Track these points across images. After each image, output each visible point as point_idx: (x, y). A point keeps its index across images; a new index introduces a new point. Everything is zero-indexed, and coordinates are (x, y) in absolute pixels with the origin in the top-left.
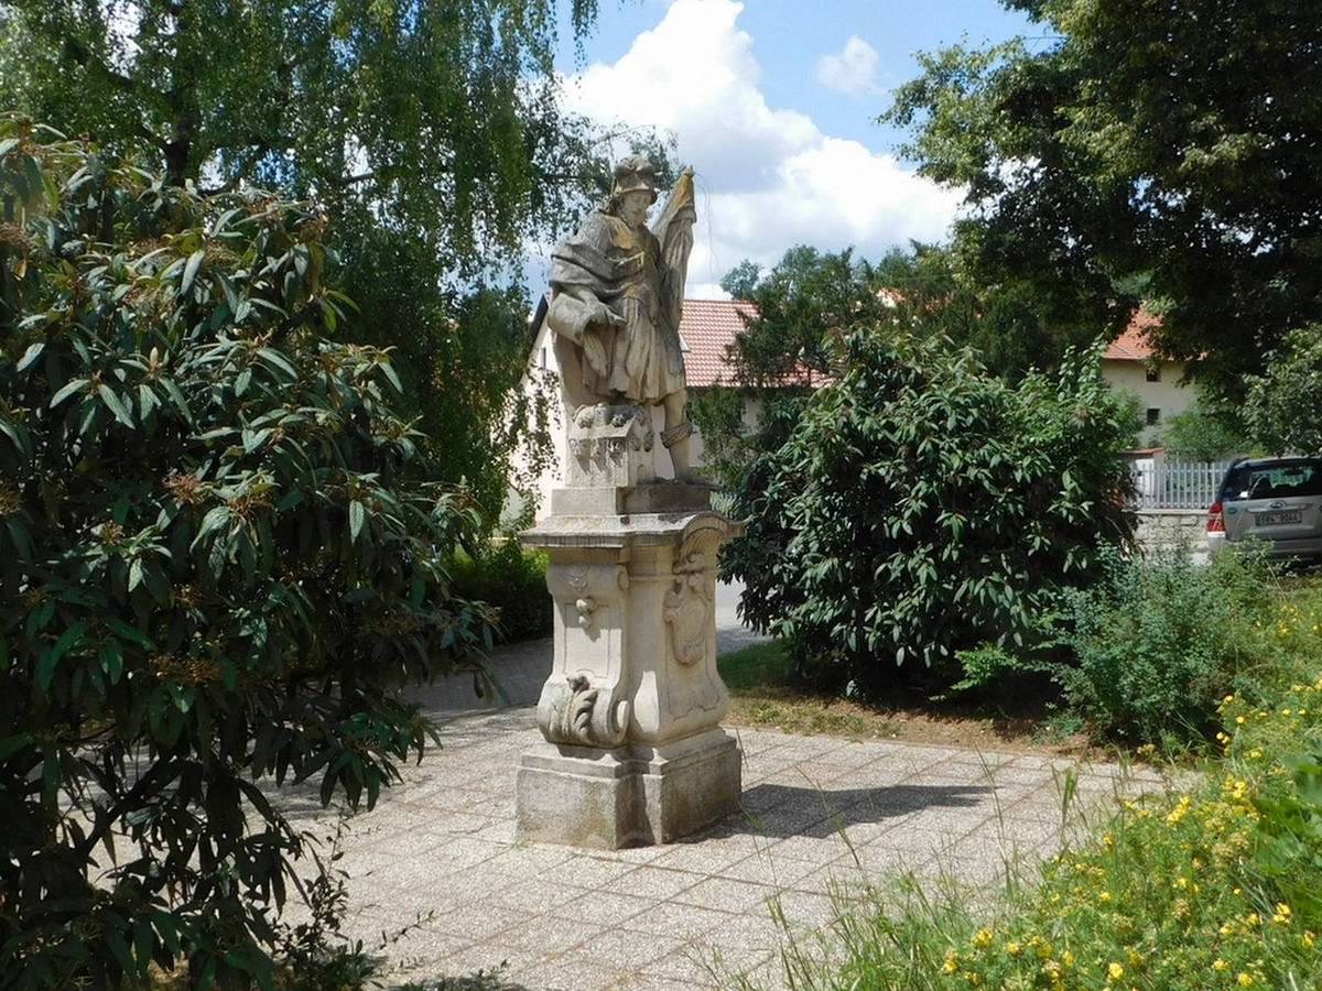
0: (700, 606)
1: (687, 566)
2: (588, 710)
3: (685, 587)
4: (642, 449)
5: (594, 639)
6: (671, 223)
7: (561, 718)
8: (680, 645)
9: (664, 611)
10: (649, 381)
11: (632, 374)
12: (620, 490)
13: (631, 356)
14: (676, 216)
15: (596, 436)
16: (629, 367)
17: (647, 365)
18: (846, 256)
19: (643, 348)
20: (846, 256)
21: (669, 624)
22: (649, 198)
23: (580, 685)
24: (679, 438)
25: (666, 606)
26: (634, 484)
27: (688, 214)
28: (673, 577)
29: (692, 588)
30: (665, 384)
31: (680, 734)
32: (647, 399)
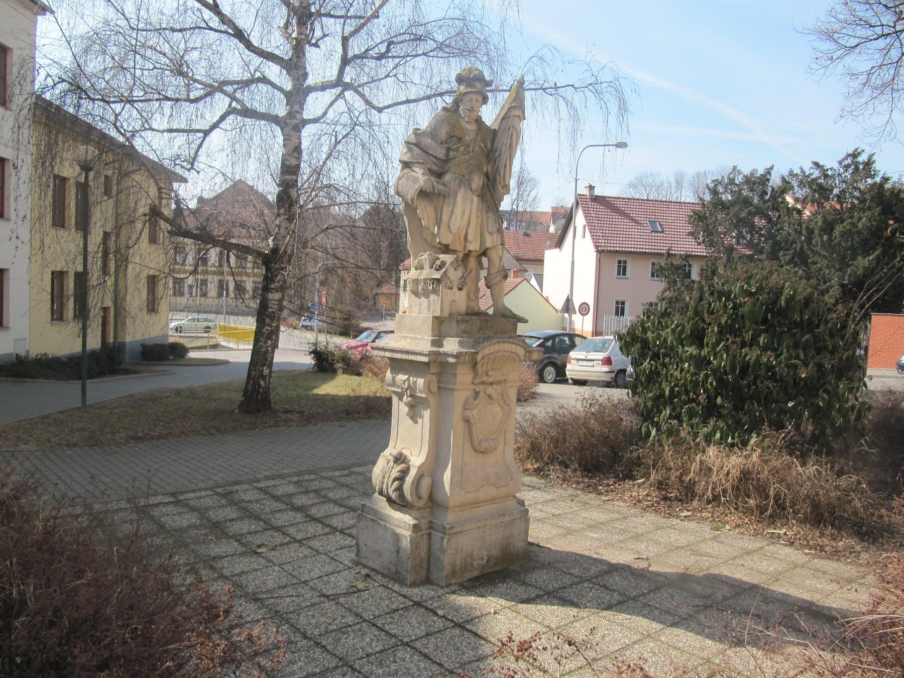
0: (497, 409)
1: (485, 379)
2: (401, 478)
3: (482, 394)
4: (455, 289)
5: (416, 422)
6: (503, 119)
7: (383, 483)
8: (477, 437)
9: (463, 412)
10: (470, 238)
11: (454, 231)
12: (435, 318)
13: (453, 218)
14: (506, 114)
15: (422, 277)
16: (452, 227)
17: (469, 225)
18: (768, 172)
19: (463, 213)
20: (768, 172)
21: (467, 421)
22: (480, 98)
23: (400, 459)
24: (495, 281)
25: (465, 408)
26: (446, 314)
27: (517, 112)
28: (474, 387)
29: (490, 397)
30: (485, 241)
31: (472, 504)
32: (470, 251)
